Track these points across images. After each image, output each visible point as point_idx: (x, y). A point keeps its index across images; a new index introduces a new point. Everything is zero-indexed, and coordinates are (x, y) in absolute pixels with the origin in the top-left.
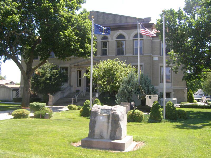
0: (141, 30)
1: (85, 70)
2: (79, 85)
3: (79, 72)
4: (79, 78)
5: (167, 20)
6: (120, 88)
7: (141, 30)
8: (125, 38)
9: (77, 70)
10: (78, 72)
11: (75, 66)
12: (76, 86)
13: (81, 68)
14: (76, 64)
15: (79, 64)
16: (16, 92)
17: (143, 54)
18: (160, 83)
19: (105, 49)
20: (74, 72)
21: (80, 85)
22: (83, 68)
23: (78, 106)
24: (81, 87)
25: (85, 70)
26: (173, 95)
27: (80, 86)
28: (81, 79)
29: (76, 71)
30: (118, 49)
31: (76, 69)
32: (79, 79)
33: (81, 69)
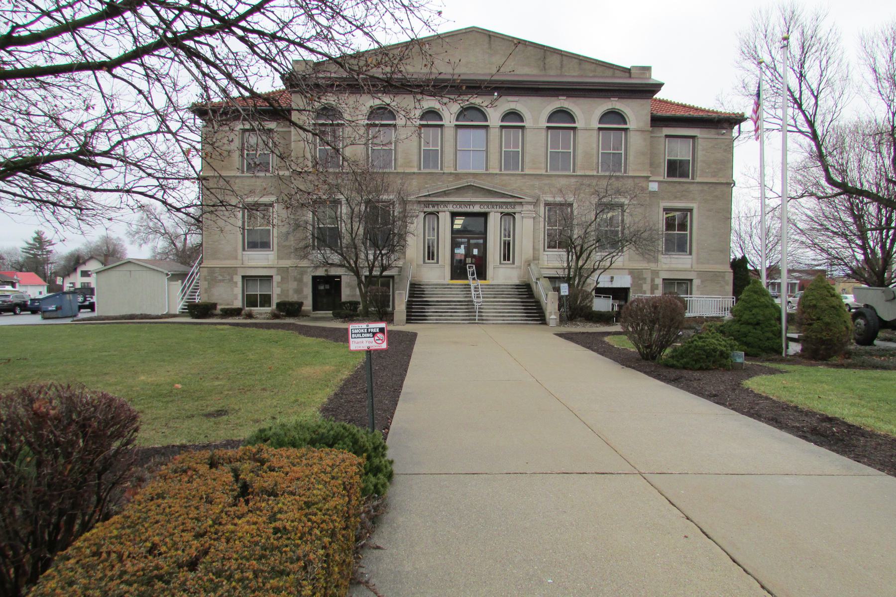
8: (522, 120)
16: (183, 283)
17: (522, 170)
26: (727, 284)
33: (436, 209)
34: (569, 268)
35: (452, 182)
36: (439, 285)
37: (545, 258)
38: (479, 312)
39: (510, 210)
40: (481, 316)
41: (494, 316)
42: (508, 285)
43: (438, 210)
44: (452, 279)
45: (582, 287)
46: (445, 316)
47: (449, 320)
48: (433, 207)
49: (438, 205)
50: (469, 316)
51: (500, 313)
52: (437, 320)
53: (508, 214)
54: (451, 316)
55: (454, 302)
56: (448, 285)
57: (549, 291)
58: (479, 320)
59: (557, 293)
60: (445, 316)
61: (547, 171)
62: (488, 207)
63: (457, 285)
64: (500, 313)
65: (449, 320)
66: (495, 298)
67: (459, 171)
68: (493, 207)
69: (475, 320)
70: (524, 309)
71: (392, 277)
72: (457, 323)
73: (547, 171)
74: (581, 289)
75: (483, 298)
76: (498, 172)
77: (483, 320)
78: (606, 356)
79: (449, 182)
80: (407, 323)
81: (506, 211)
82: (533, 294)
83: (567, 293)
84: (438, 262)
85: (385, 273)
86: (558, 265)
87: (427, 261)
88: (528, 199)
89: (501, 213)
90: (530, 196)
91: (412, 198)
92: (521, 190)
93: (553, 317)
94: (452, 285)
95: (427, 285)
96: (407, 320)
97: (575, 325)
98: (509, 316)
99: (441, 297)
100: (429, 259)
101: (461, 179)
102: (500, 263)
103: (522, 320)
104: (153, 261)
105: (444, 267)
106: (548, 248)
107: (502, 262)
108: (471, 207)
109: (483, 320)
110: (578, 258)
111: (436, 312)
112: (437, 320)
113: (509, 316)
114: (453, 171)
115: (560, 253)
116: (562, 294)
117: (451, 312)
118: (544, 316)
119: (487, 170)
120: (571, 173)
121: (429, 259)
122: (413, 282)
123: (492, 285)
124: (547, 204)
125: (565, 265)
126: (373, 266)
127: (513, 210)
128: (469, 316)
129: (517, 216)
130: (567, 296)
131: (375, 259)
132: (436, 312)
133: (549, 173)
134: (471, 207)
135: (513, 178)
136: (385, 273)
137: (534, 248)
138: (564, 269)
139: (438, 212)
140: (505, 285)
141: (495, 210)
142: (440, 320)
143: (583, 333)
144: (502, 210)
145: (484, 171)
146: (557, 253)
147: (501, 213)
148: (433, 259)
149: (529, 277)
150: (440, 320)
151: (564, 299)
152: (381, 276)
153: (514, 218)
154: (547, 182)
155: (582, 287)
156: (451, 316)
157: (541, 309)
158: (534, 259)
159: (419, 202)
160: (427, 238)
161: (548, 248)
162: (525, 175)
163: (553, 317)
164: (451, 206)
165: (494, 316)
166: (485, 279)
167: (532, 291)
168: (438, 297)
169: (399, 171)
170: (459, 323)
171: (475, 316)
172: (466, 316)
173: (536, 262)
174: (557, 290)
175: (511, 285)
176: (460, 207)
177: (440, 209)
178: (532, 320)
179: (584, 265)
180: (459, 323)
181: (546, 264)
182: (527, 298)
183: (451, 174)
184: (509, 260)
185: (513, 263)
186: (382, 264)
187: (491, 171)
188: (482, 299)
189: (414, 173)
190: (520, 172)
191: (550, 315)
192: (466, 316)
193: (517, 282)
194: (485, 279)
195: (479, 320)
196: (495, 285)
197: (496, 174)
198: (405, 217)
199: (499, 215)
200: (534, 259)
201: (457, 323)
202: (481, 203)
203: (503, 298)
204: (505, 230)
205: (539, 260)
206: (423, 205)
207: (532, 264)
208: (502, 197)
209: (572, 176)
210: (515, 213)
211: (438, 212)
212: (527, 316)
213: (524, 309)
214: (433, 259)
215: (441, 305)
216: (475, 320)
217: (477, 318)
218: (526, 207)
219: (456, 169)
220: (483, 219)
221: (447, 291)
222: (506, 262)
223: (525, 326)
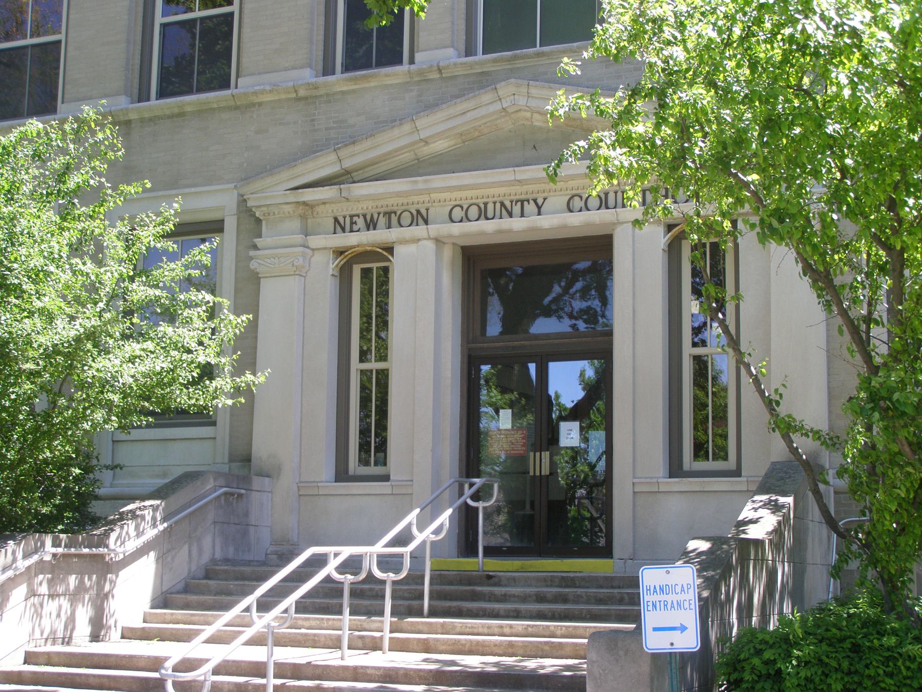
0: (535, 472)
1: (439, 241)
2: (364, 462)
3: (366, 273)
5: (629, 151)
6: (858, 58)
7: (535, 472)
9: (339, 252)
10: (344, 273)
11: (310, 195)
12: (327, 470)
13: (388, 214)
14: (326, 165)
15: (353, 157)
19: (198, 14)
20: (300, 273)
21: (382, 447)
22: (421, 217)
23: (568, 411)
24: (386, 478)
27: (373, 470)
28: (383, 377)
30: (164, 26)
31: (316, 241)
33: (380, 235)
83: (689, 641)
100: (364, 462)
130: (684, 657)
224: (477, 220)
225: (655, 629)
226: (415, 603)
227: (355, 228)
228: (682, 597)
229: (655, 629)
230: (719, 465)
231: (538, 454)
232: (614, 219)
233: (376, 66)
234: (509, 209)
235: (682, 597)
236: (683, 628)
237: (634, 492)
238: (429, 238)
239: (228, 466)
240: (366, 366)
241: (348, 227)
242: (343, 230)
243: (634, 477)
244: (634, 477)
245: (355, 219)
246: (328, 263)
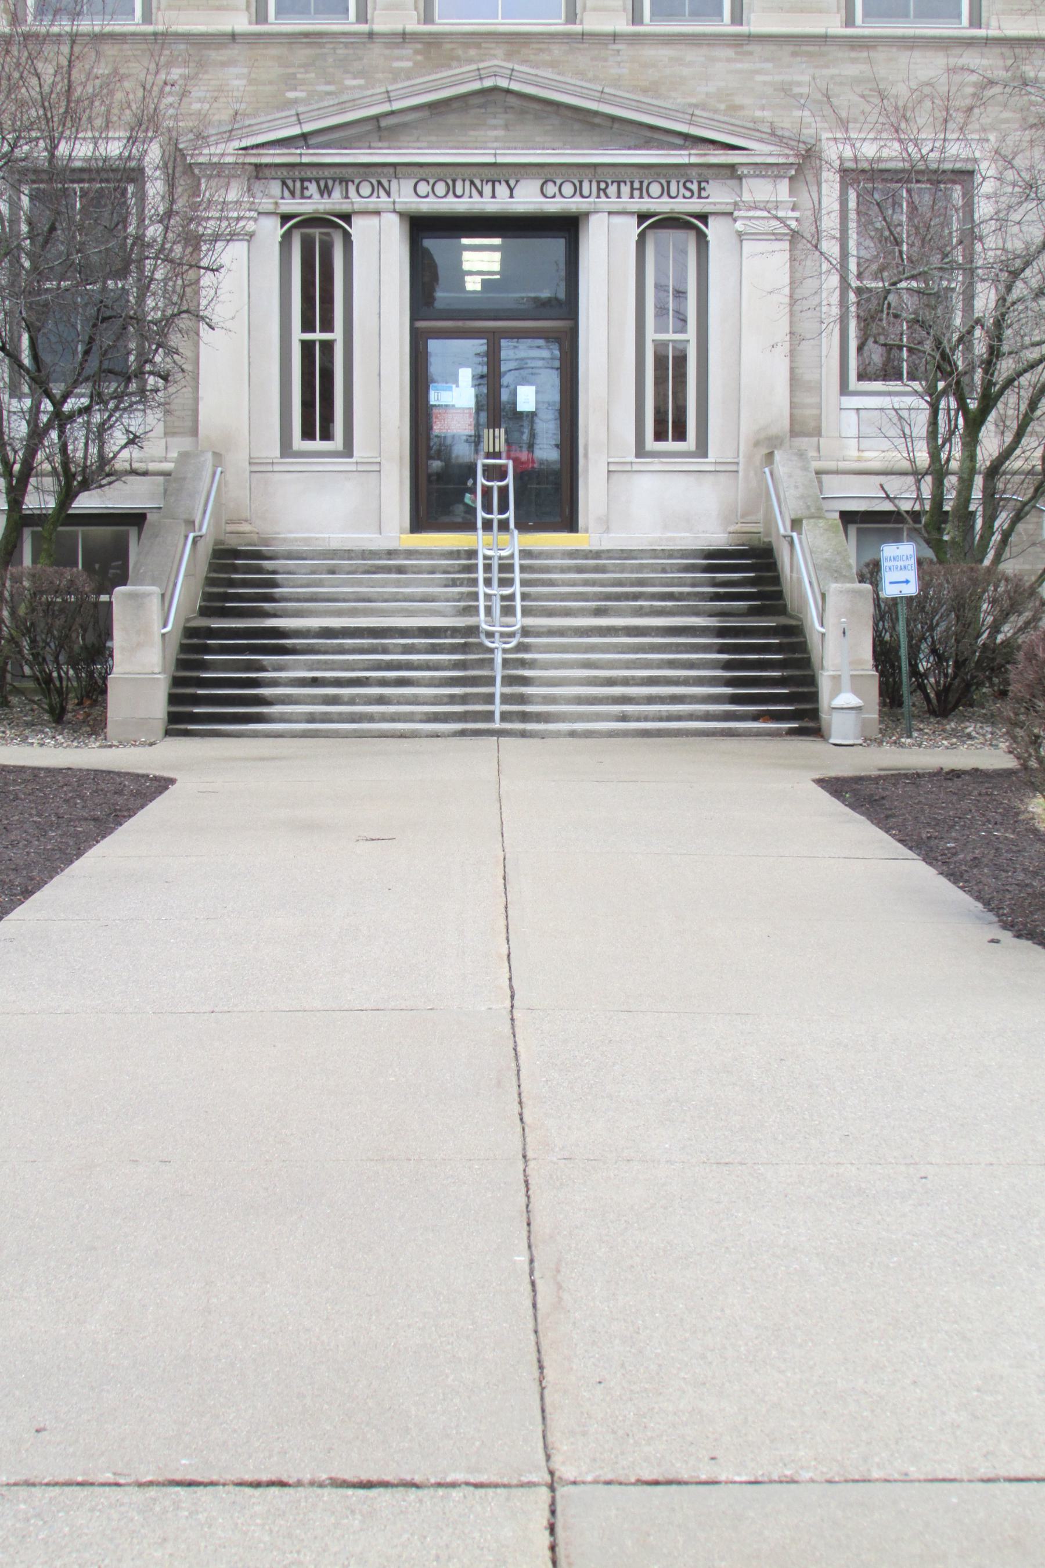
4: (308, 325)
17: (737, 18)
18: (844, 390)
25: (401, 214)
29: (271, 231)
32: (307, 347)
33: (335, 202)
34: (938, 471)
35: (409, 75)
36: (348, 554)
37: (849, 423)
38: (508, 681)
39: (683, 205)
40: (522, 699)
41: (580, 700)
42: (670, 554)
43: (345, 207)
44: (419, 523)
45: (998, 559)
46: (352, 701)
47: (370, 718)
48: (325, 191)
49: (344, 181)
50: (464, 699)
51: (611, 682)
52: (312, 718)
53: (672, 222)
54: (381, 700)
55: (403, 632)
56: (390, 554)
57: (838, 575)
58: (505, 717)
59: (867, 587)
60: (352, 701)
61: (850, 22)
62: (578, 191)
63: (429, 554)
64: (611, 682)
65: (370, 718)
66: (599, 612)
67: (442, 24)
68: (602, 191)
69: (489, 716)
70: (728, 665)
71: (137, 519)
72: (402, 735)
73: (850, 22)
74: (989, 570)
75: (526, 612)
76: (622, 25)
77: (525, 717)
78: (85, 851)
79: (396, 75)
80: (168, 733)
81: (663, 205)
82: (779, 595)
83: (911, 589)
84: (348, 450)
85: (86, 502)
86: (898, 459)
87: (651, 444)
88: (763, 151)
89: (642, 217)
90: (774, 136)
91: (227, 151)
92: (734, 108)
93: (847, 699)
94: (410, 554)
95: (290, 556)
96: (173, 718)
97: (954, 733)
98: (650, 700)
99: (353, 613)
100: (308, 434)
101: (451, 60)
102: (641, 451)
103: (708, 717)
104: (443, 451)
105: (375, 469)
106: (861, 377)
107: (651, 444)
108: (502, 190)
109: (525, 717)
110: (975, 423)
111: (315, 682)
112: (312, 718)
113: (650, 700)
114: (413, 25)
115: (898, 402)
116: (889, 591)
117: (383, 683)
118: (813, 697)
119: (572, 17)
120: (963, 28)
121: (308, 434)
122: (233, 542)
123: (597, 554)
124: (849, 175)
125: (923, 457)
126: (28, 469)
127: (695, 205)
128: (464, 699)
129: (714, 230)
130: (910, 599)
131: (36, 435)
132: (315, 682)
133: (862, 28)
134: (502, 190)
135: (694, 55)
136: (86, 502)
137: (795, 381)
138: (918, 475)
139: (347, 218)
140: (654, 553)
141: (612, 202)
142: (326, 718)
143: (955, 774)
144: (646, 205)
145: (558, 25)
146: (884, 402)
147: (642, 217)
148: (327, 435)
149: (769, 520)
150: (326, 718)
151: (902, 611)
152: (64, 516)
153: (702, 240)
154: (851, 70)
155: (998, 559)
156: (381, 700)
157: (806, 663)
158: (794, 433)
159: (259, 171)
160: (651, 335)
161: (861, 377)
162: (750, 38)
163: (847, 699)
164: (407, 185)
165: (580, 700)
166: (571, 524)
167: (777, 580)
168: (339, 613)
169: (378, 27)
170: (414, 735)
171: (489, 699)
172: (452, 699)
173: (803, 442)
174: (871, 573)
175: (684, 554)
176: (451, 190)
177: (357, 201)
178: (756, 717)
179: (1006, 454)
180: (414, 735)
181: (851, 453)
182: (752, 612)
183: (404, 37)
184: (680, 434)
185: (702, 450)
186: (66, 462)
187: (591, 23)
188: (519, 621)
189: (234, 36)
190: (725, 26)
191: (836, 692)
192: (452, 699)
193: (717, 537)
194: (571, 524)
195: (505, 717)
196: (609, 554)
197: (615, 37)
198: (194, 241)
199: (631, 228)
200: (795, 431)
201: (402, 735)
202: (546, 173)
203: (639, 612)
204: (660, 287)
205: (818, 432)
206: (275, 188)
207: (778, 456)
208: (646, 144)
209: (969, 43)
210: (703, 218)
211: (347, 218)
212: (735, 699)
213: (728, 665)
214: (327, 435)
215: (342, 650)
216: (489, 716)
217: (498, 689)
218: (758, 190)
219: (428, 17)
220: (557, 246)
221: (385, 585)
222: (670, 445)
223: (466, 741)
224: (445, 196)
225: (891, 583)
226: (527, 576)
227: (307, 193)
228: (906, 563)
229: (891, 583)
230: (679, 446)
231: (491, 431)
232: (592, 208)
233: (317, 12)
234: (480, 188)
235: (906, 563)
236: (907, 582)
237: (609, 471)
238: (395, 211)
239: (164, 440)
240: (326, 336)
241: (298, 192)
242: (293, 194)
243: (609, 457)
244: (609, 457)
245: (306, 184)
246: (276, 229)
